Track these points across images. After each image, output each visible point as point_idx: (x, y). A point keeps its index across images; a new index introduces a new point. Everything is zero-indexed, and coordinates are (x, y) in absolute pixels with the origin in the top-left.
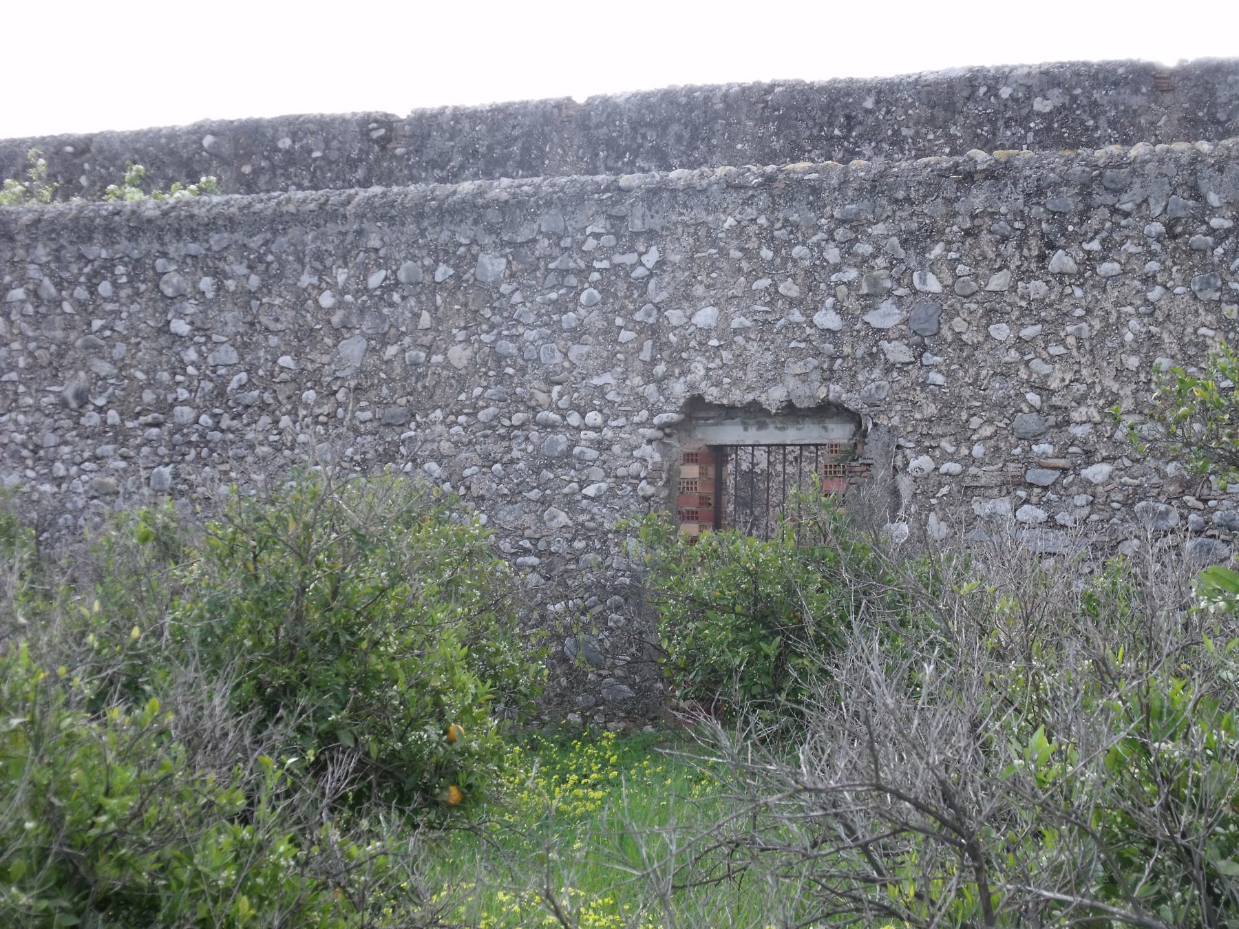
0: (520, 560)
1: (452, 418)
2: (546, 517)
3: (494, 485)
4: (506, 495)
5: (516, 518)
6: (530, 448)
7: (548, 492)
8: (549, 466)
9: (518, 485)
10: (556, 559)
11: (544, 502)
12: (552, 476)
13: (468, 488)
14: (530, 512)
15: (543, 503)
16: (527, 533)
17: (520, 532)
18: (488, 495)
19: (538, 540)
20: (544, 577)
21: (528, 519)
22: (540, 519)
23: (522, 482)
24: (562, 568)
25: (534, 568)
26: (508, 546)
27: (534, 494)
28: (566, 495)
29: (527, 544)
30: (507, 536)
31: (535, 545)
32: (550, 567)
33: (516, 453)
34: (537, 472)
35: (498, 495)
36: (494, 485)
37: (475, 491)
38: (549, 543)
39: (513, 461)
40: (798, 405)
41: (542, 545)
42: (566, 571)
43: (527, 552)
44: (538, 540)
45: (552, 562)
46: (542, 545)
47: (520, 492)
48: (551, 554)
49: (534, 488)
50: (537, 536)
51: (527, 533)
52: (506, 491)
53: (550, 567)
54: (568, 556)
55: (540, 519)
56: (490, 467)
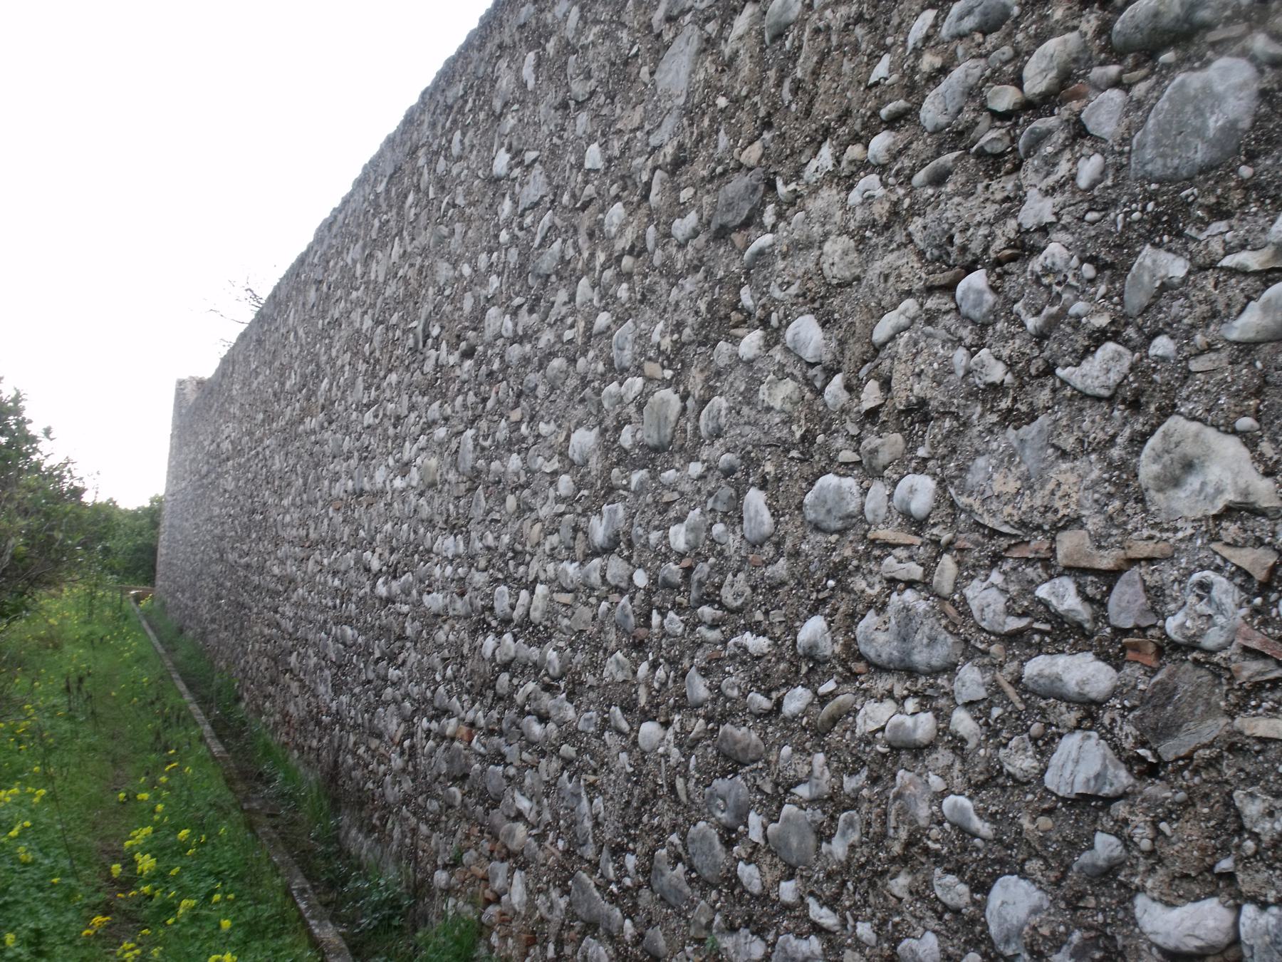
0: (1036, 667)
1: (855, 151)
2: (1148, 468)
3: (960, 356)
4: (996, 389)
5: (1028, 483)
6: (1089, 168)
7: (1162, 346)
8: (1167, 225)
9: (1041, 337)
10: (1188, 678)
11: (1141, 400)
12: (1177, 268)
13: (886, 384)
14: (1085, 447)
15: (1135, 405)
16: (1069, 545)
17: (1039, 543)
18: (936, 397)
19: (1111, 577)
20: (1131, 761)
21: (1074, 484)
22: (1123, 482)
23: (1054, 321)
24: (1214, 727)
25: (1090, 711)
26: (997, 602)
27: (1101, 369)
28: (1246, 348)
29: (1065, 597)
30: (996, 559)
31: (1098, 604)
32: (1159, 717)
33: (1037, 209)
34: (1111, 264)
35: (973, 394)
36: (960, 356)
37: (908, 389)
38: (1156, 595)
39: (1024, 248)
40: (922, 114)
41: (1126, 604)
42: (1235, 746)
43: (1065, 633)
44: (1111, 577)
45: (1166, 693)
46: (1126, 604)
47: (1049, 370)
48: (1168, 648)
49: (1099, 337)
50: (1106, 561)
51: (1069, 545)
52: (997, 373)
53: (1159, 717)
54: (1250, 670)
55: (1123, 482)
56: (950, 288)
